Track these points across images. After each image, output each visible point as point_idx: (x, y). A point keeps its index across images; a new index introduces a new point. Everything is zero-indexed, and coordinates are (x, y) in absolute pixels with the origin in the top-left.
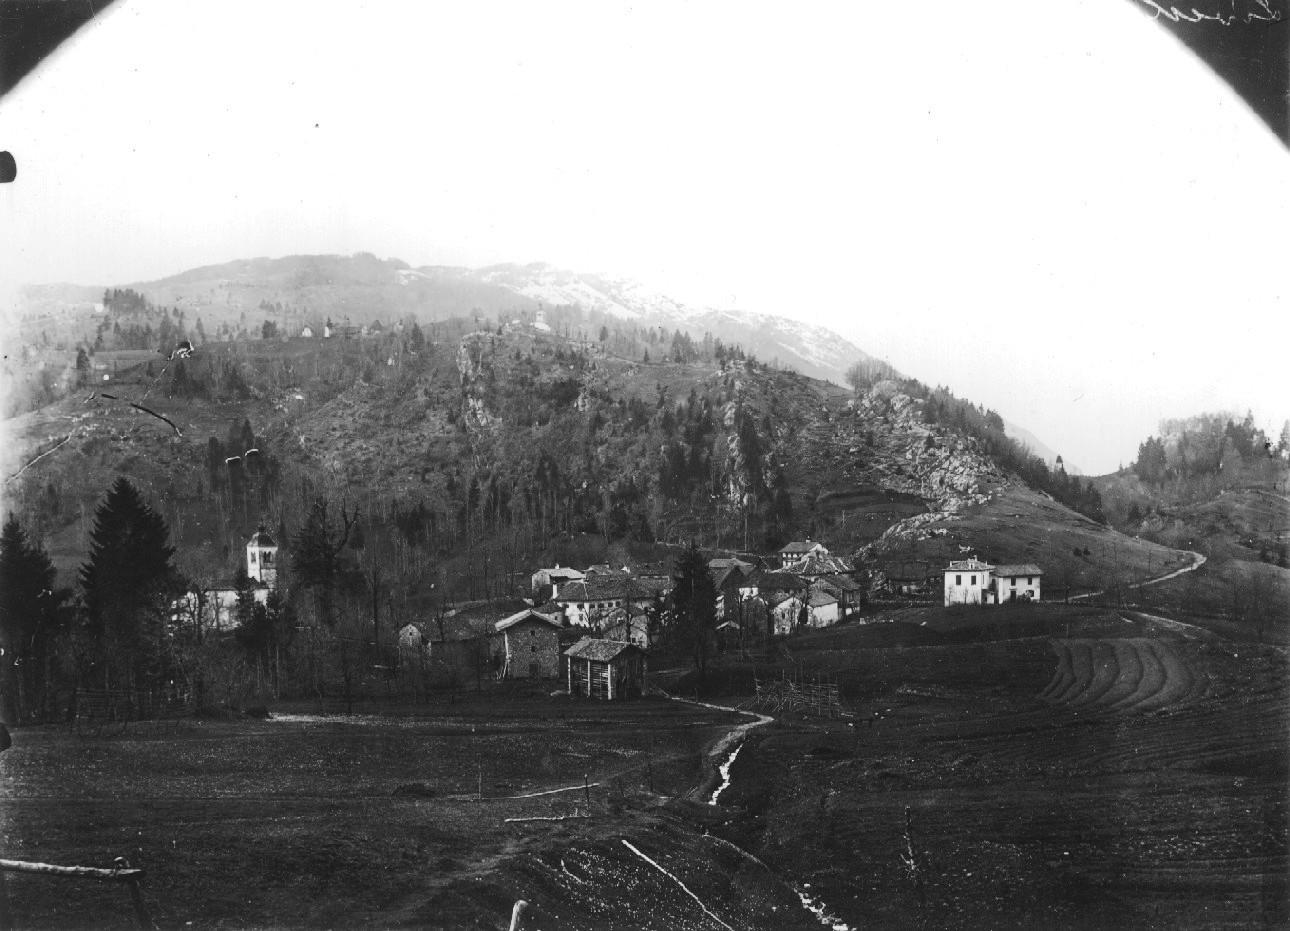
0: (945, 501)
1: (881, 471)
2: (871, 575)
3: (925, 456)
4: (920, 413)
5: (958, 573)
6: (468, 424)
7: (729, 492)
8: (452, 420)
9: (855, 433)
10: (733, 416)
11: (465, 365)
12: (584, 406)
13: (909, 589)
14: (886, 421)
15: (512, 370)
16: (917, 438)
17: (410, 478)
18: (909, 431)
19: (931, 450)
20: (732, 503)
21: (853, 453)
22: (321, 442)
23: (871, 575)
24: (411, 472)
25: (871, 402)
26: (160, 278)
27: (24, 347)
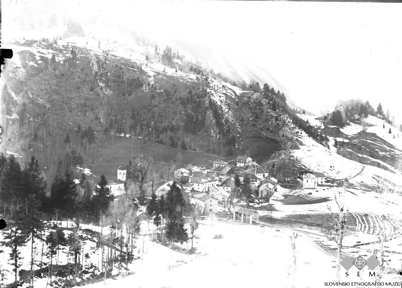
0: (285, 143)
1: (261, 128)
2: (275, 174)
3: (275, 124)
4: (271, 107)
5: (308, 179)
6: (99, 93)
7: (211, 133)
8: (92, 90)
9: (250, 112)
10: (208, 103)
11: (95, 68)
12: (146, 90)
13: (288, 180)
14: (260, 109)
15: (115, 71)
16: (272, 117)
17: (79, 114)
18: (269, 113)
19: (278, 122)
20: (212, 137)
21: (250, 120)
22: (38, 95)
23: (275, 174)
24: (79, 111)
25: (254, 100)
26: (380, 137)
27: (57, 175)
